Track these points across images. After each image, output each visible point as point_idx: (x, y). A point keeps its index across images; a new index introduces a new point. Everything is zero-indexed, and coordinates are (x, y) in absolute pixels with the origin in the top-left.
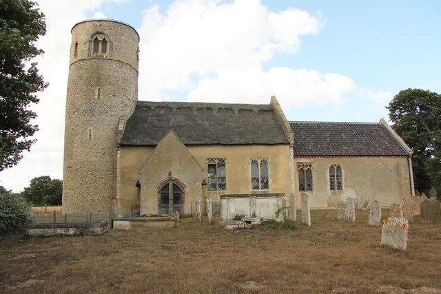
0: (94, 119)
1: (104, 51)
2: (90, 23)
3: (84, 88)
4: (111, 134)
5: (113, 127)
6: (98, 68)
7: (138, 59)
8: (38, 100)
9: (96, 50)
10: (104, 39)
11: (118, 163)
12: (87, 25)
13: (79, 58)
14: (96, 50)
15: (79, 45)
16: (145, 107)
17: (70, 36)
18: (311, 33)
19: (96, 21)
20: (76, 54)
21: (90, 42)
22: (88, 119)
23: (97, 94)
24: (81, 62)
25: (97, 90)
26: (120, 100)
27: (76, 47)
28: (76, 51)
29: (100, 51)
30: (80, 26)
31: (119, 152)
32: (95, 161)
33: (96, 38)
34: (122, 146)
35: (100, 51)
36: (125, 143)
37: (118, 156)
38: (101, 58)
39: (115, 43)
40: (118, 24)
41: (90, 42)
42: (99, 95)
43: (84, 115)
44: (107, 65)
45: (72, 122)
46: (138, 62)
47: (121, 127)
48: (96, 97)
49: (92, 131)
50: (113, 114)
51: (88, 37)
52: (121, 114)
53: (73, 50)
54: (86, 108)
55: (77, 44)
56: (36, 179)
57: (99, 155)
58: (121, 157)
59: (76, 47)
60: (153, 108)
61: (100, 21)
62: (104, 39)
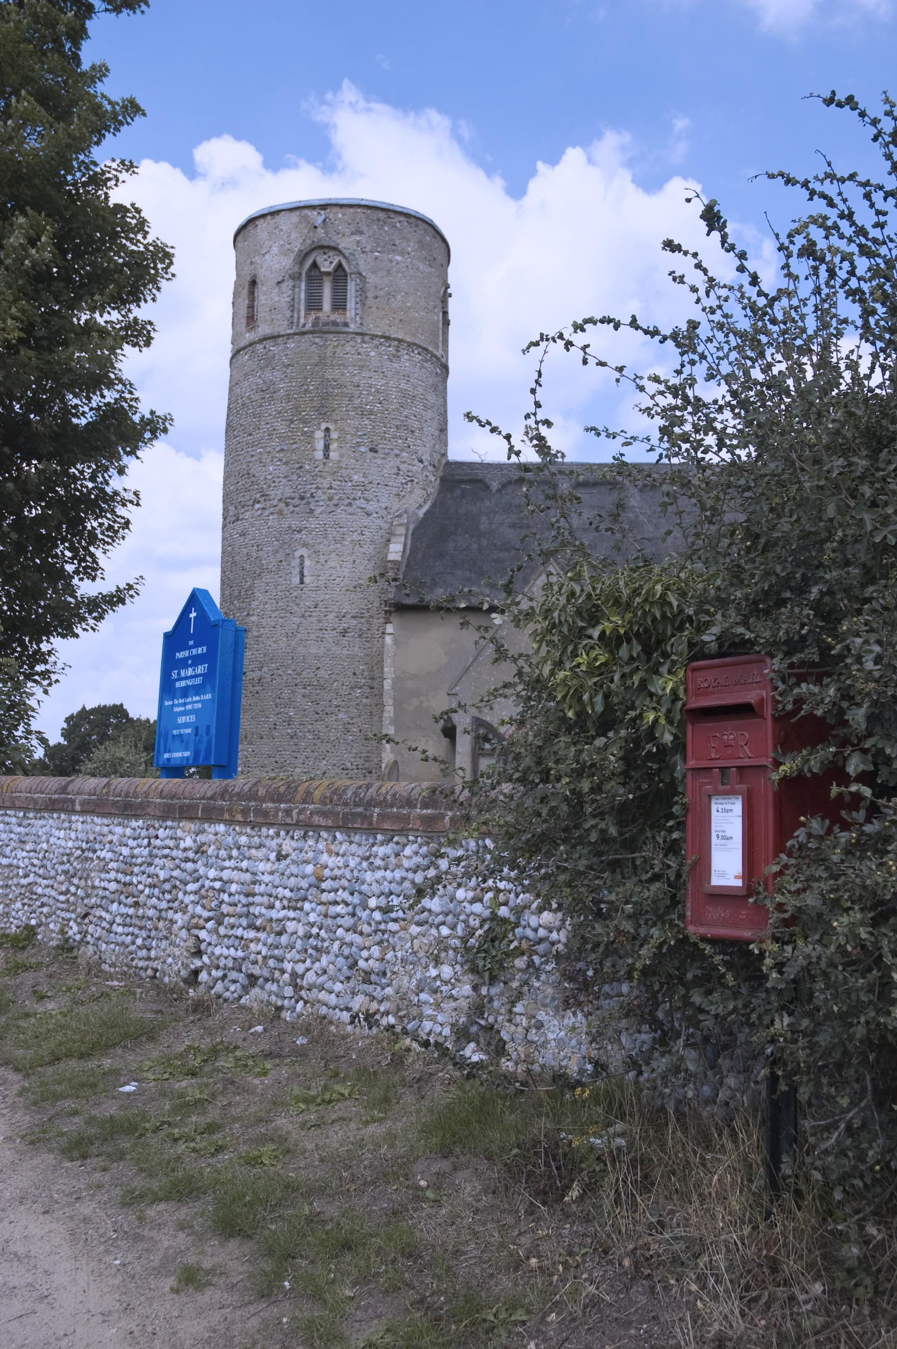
0: (312, 523)
1: (339, 305)
2: (294, 217)
3: (281, 427)
4: (366, 570)
5: (368, 549)
6: (322, 362)
7: (446, 323)
8: (568, 350)
9: (314, 304)
10: (340, 266)
11: (388, 662)
12: (287, 222)
13: (264, 329)
14: (314, 304)
15: (261, 290)
16: (470, 481)
17: (230, 256)
18: (132, 453)
19: (312, 207)
20: (251, 319)
21: (295, 277)
22: (294, 524)
23: (320, 445)
24: (268, 344)
25: (319, 434)
26: (392, 462)
27: (252, 293)
28: (251, 307)
29: (327, 306)
30: (260, 223)
31: (390, 628)
32: (317, 657)
33: (315, 265)
34: (399, 609)
35: (327, 306)
36: (408, 601)
37: (388, 640)
38: (336, 329)
39: (372, 279)
40: (382, 215)
41: (295, 277)
42: (327, 448)
43: (280, 513)
44: (349, 350)
45: (243, 534)
46: (445, 333)
47: (395, 551)
48: (319, 455)
49: (307, 563)
50: (370, 507)
51: (287, 262)
52: (396, 505)
53: (244, 302)
54: (288, 492)
55: (253, 283)
56: (84, 714)
57: (329, 636)
58: (396, 642)
59: (252, 293)
60: (495, 486)
61: (324, 207)
62: (340, 266)
